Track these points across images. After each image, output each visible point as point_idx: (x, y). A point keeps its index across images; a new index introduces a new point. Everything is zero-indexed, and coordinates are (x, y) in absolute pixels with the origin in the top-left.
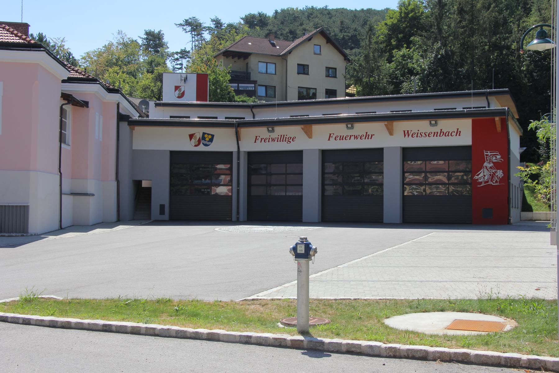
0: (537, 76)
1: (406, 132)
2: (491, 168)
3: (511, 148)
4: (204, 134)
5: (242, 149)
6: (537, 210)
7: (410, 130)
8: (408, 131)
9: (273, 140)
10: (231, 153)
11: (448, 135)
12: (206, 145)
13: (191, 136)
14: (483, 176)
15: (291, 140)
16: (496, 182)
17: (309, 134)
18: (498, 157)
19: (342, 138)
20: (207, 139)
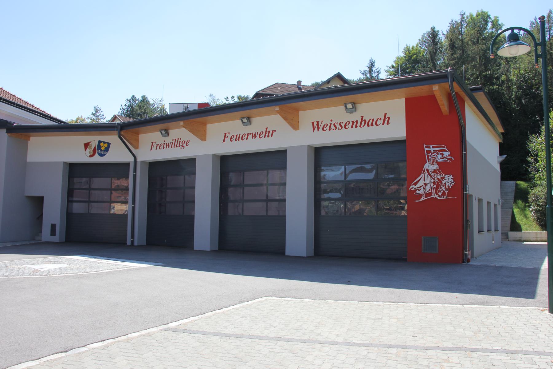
0: (526, 102)
1: (315, 124)
2: (435, 171)
3: (468, 139)
4: (100, 142)
5: (139, 159)
6: (527, 229)
7: (320, 120)
8: (318, 122)
9: (168, 146)
10: (128, 164)
11: (372, 125)
12: (101, 155)
13: (86, 145)
14: (423, 185)
15: (185, 145)
16: (444, 194)
17: (203, 136)
18: (446, 154)
19: (238, 138)
20: (103, 148)
